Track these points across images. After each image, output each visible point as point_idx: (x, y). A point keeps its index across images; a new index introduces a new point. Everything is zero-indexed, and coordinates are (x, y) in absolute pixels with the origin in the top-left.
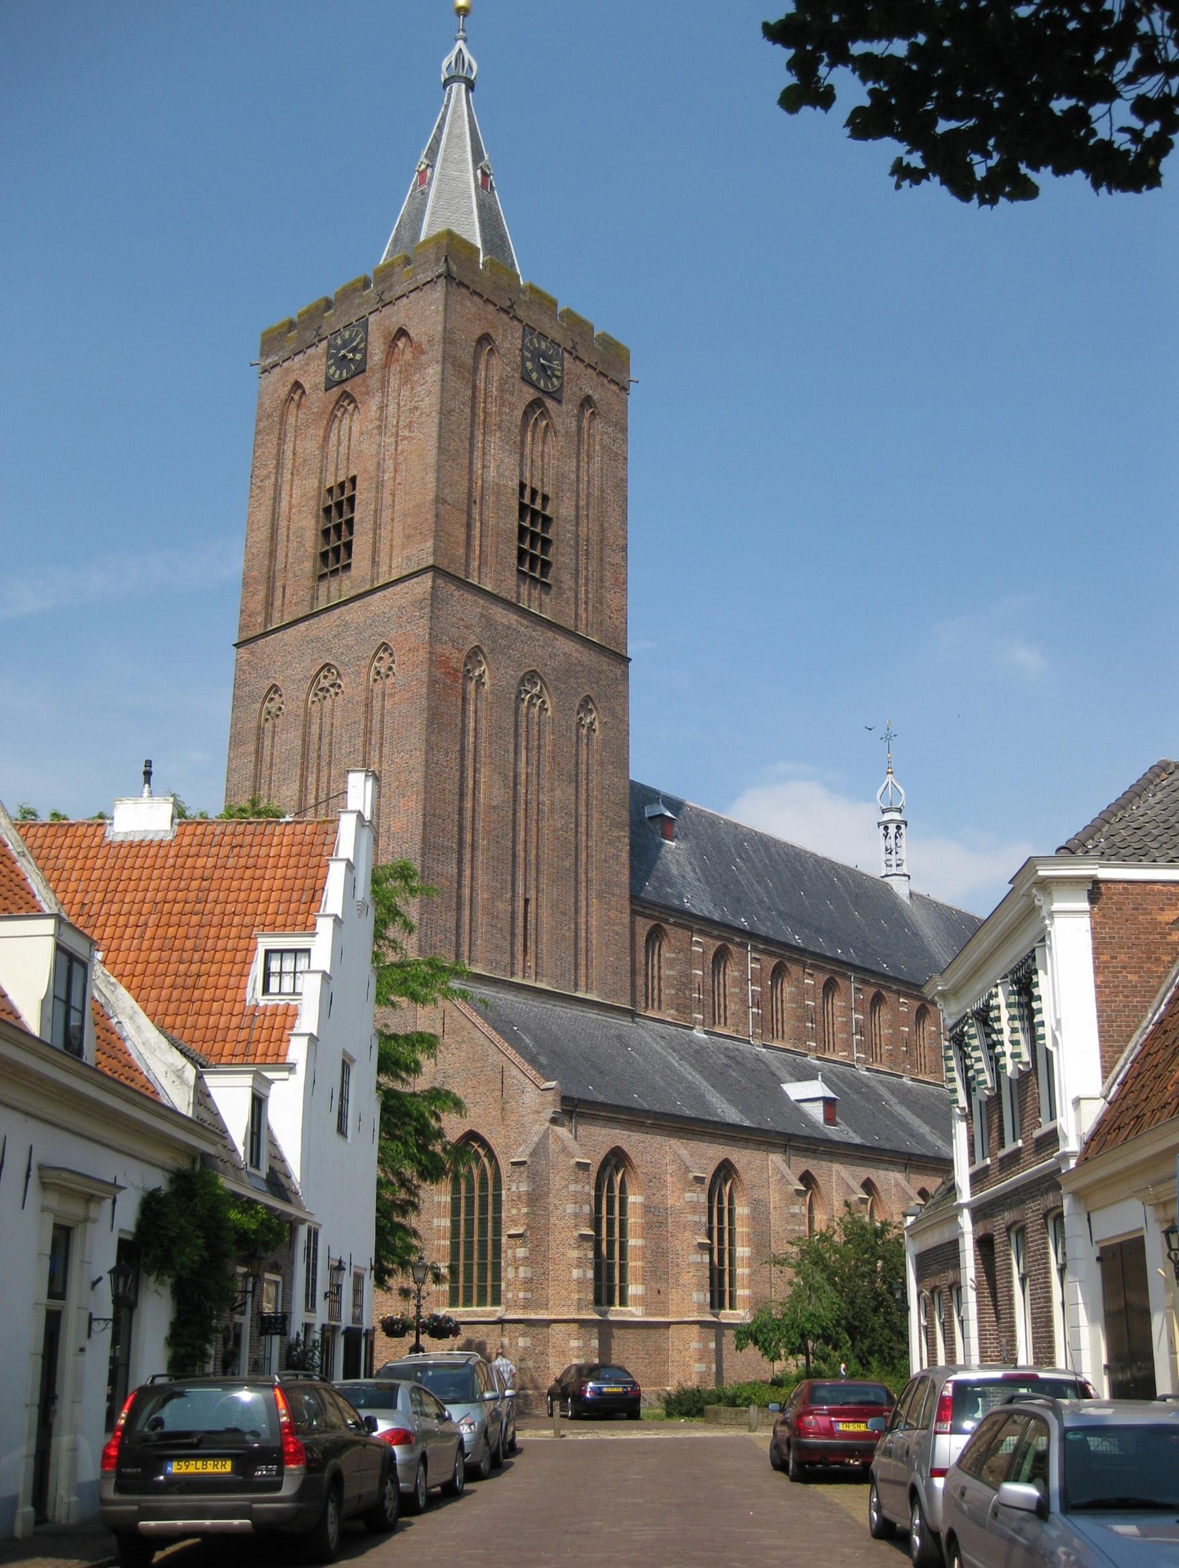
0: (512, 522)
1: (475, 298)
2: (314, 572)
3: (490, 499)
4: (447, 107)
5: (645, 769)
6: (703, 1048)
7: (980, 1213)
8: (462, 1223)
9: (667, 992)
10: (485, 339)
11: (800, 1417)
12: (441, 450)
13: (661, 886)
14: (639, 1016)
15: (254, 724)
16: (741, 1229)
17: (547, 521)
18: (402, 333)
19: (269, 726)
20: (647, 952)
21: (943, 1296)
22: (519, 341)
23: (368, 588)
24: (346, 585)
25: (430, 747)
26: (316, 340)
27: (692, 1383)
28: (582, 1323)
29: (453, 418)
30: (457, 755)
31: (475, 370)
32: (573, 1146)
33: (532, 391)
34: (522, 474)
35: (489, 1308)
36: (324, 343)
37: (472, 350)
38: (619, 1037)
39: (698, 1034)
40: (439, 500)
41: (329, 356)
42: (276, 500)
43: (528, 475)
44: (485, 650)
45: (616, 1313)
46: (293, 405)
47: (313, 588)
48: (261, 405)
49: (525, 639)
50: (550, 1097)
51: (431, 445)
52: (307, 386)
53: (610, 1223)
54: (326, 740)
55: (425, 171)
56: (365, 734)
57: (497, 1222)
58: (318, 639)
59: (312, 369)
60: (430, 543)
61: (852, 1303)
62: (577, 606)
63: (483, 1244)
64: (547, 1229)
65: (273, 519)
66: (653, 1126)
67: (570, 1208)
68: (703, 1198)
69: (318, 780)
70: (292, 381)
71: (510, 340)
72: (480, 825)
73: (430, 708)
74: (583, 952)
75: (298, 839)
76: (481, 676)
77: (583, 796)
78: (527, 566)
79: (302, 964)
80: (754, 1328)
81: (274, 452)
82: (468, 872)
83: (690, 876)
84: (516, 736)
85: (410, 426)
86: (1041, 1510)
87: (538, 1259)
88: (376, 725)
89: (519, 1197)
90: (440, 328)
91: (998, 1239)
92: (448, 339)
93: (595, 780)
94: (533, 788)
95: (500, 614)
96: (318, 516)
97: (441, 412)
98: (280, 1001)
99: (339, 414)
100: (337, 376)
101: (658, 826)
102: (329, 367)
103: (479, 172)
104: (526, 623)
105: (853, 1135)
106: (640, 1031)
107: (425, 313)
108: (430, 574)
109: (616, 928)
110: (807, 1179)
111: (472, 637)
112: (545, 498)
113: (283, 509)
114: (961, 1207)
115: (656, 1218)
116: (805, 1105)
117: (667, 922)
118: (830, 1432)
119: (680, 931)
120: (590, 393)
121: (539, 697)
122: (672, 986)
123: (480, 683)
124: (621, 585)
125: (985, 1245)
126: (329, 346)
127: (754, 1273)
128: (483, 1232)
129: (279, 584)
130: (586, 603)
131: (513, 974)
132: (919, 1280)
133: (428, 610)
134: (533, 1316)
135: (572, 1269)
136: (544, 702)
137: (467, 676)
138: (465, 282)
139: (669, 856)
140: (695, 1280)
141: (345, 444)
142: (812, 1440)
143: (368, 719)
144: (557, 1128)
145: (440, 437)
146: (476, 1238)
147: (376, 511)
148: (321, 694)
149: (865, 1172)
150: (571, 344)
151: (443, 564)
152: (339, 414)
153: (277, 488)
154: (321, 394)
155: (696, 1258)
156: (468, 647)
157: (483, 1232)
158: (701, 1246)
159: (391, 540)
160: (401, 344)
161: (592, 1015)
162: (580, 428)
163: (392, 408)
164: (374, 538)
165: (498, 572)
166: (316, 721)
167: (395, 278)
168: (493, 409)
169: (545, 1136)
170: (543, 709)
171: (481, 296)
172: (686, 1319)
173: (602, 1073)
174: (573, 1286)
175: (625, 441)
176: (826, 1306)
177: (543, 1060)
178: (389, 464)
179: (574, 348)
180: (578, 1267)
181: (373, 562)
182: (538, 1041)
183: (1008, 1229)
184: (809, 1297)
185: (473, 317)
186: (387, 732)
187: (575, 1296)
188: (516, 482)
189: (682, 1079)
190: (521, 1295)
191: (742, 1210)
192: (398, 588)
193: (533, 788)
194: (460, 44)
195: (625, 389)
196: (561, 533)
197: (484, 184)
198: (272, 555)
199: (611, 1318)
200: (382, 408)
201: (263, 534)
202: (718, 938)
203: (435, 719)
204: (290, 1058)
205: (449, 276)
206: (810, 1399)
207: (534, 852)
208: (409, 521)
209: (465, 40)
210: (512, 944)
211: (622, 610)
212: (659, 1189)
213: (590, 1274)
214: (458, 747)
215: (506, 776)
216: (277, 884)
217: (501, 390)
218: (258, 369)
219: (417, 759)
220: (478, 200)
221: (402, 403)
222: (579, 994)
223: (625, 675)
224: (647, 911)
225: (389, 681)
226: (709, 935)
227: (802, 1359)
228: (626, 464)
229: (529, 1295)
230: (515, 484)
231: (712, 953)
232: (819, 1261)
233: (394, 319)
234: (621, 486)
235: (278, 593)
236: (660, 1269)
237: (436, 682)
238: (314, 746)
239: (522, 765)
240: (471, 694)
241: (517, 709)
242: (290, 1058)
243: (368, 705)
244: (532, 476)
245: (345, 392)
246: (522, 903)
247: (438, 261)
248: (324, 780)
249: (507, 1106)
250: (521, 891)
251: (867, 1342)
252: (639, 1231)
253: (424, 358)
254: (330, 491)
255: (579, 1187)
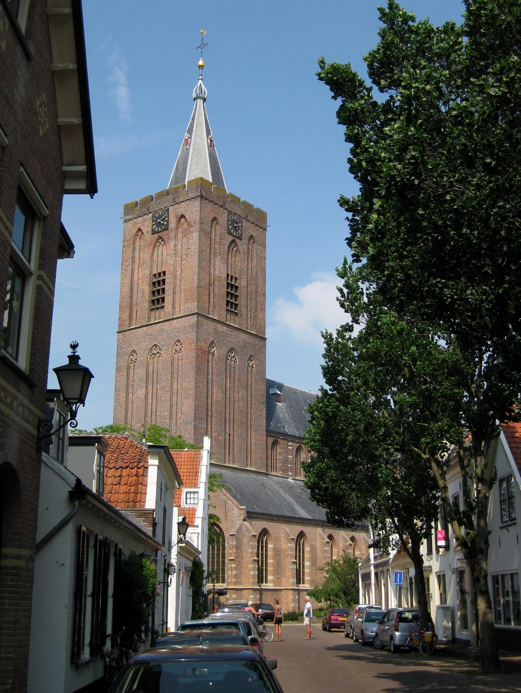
0: (224, 291)
1: (211, 203)
2: (149, 308)
3: (217, 283)
4: (195, 109)
5: (270, 375)
6: (292, 486)
7: (376, 566)
8: (211, 554)
9: (279, 465)
10: (215, 219)
11: (330, 616)
12: (199, 267)
13: (277, 423)
14: (269, 474)
15: (126, 364)
16: (307, 556)
17: (237, 288)
18: (183, 216)
20: (272, 451)
21: (367, 586)
22: (227, 218)
24: (162, 315)
25: (197, 381)
26: (147, 213)
27: (291, 610)
28: (254, 590)
29: (203, 253)
30: (206, 383)
31: (211, 232)
32: (251, 529)
33: (231, 237)
34: (227, 271)
35: (220, 584)
36: (151, 214)
37: (210, 225)
38: (263, 485)
39: (290, 480)
40: (199, 287)
41: (153, 221)
42: (132, 275)
43: (230, 271)
44: (215, 342)
45: (264, 586)
46: (138, 237)
47: (149, 314)
48: (124, 235)
50: (243, 512)
51: (196, 263)
53: (262, 554)
54: (155, 374)
55: (187, 139)
56: (171, 373)
57: (224, 554)
58: (151, 334)
59: (146, 224)
60: (196, 303)
61: (345, 584)
62: (247, 320)
63: (218, 562)
64: (242, 557)
65: (131, 283)
66: (277, 520)
67: (250, 550)
68: (294, 546)
69: (152, 389)
70: (138, 227)
71: (223, 218)
72: (214, 408)
73: (197, 367)
74: (249, 452)
75: (190, 456)
76: (214, 352)
77: (249, 393)
78: (230, 307)
79: (196, 496)
80: (314, 592)
81: (131, 256)
82: (209, 426)
83: (287, 417)
84: (226, 373)
85: (187, 255)
86: (362, 622)
87: (239, 567)
88: (175, 370)
89: (233, 546)
90: (198, 218)
91: (379, 574)
92: (201, 222)
93: (254, 386)
94: (232, 392)
95: (221, 328)
96: (150, 285)
97: (199, 252)
98: (191, 506)
99: (158, 245)
100: (157, 229)
101: (275, 398)
102: (153, 225)
103: (209, 140)
104: (229, 329)
106: (270, 481)
107: (193, 210)
108: (196, 316)
109: (261, 442)
110: (330, 537)
111: (211, 338)
112: (236, 279)
113: (135, 279)
114: (371, 564)
115: (278, 552)
117: (279, 438)
118: (337, 620)
119: (284, 441)
120: (252, 234)
121: (234, 357)
122: (281, 462)
123: (213, 355)
124: (263, 310)
125: (376, 574)
126: (153, 216)
127: (311, 571)
128: (218, 558)
130: (251, 318)
131: (225, 462)
132: (362, 581)
133: (195, 329)
134: (237, 587)
135: (251, 571)
136: (235, 359)
137: (209, 353)
138: (207, 197)
139: (279, 410)
140: (291, 574)
141: (160, 257)
142: (333, 622)
143: (172, 368)
144: (245, 522)
145: (199, 261)
146: (216, 560)
147: (174, 287)
148: (153, 356)
149: (352, 534)
150: (245, 215)
152: (158, 245)
153: (133, 270)
154: (150, 235)
155: (291, 567)
156: (209, 342)
157: (218, 558)
158: (293, 562)
161: (253, 476)
162: (248, 248)
163: (179, 246)
164: (173, 298)
165: (219, 312)
167: (180, 193)
168: (217, 246)
169: (241, 525)
170: (235, 362)
171: (213, 202)
172: (288, 588)
173: (258, 500)
174: (251, 577)
175: (265, 251)
176: (336, 585)
177: (238, 497)
178: (179, 269)
179: (246, 216)
180: (253, 570)
181: (173, 307)
182: (236, 489)
183: (381, 572)
184: (331, 583)
185: (211, 210)
186: (180, 373)
187: (252, 580)
188: (226, 275)
189: (286, 500)
190: (233, 580)
191: (307, 549)
192: (184, 319)
193: (232, 392)
194: (200, 82)
195: (265, 230)
196: (242, 293)
197: (211, 145)
198: (131, 298)
199: (263, 588)
200: (175, 246)
201: (127, 289)
203: (198, 370)
204: (196, 524)
205: (202, 197)
206: (332, 613)
207: (232, 416)
208: (187, 293)
209: (202, 80)
210: (225, 451)
211: (264, 319)
212: (279, 542)
213: (257, 573)
214: (206, 380)
215: (223, 389)
216: (185, 470)
217: (220, 239)
218: (122, 220)
219: (192, 385)
220: (209, 152)
221: (183, 245)
222: (248, 468)
223: (265, 345)
225: (180, 354)
227: (329, 602)
228: (265, 260)
229: (236, 580)
230: (225, 276)
232: (334, 570)
233: (180, 210)
234: (264, 269)
235: (134, 313)
236: (279, 570)
237: (199, 356)
238: (150, 376)
239: (228, 384)
240: (210, 360)
241: (226, 362)
242: (196, 524)
243: (172, 362)
244: (231, 271)
245: (160, 236)
246: (228, 436)
247: (197, 189)
248: (155, 389)
250: (228, 431)
251: (350, 597)
252: (272, 557)
254: (155, 275)
255: (253, 543)
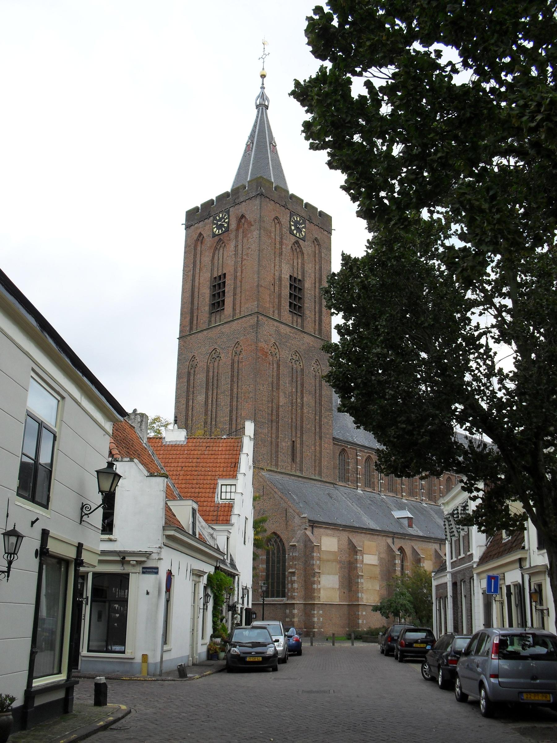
18: (243, 216)
19: (192, 371)
23: (231, 319)
39: (359, 491)
46: (199, 243)
49: (292, 338)
52: (205, 235)
54: (215, 378)
69: (212, 394)
70: (199, 232)
81: (192, 261)
85: (247, 254)
88: (235, 374)
96: (210, 288)
105: (419, 531)
116: (401, 520)
129: (195, 315)
151: (261, 310)
159: (241, 300)
160: (243, 221)
166: (211, 370)
167: (240, 194)
178: (239, 269)
200: (236, 246)
202: (367, 453)
224: (340, 444)
226: (364, 452)
231: (365, 458)
233: (240, 211)
248: (215, 394)
249: (288, 523)
253: (252, 228)
